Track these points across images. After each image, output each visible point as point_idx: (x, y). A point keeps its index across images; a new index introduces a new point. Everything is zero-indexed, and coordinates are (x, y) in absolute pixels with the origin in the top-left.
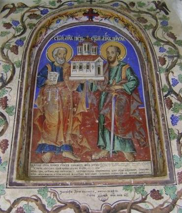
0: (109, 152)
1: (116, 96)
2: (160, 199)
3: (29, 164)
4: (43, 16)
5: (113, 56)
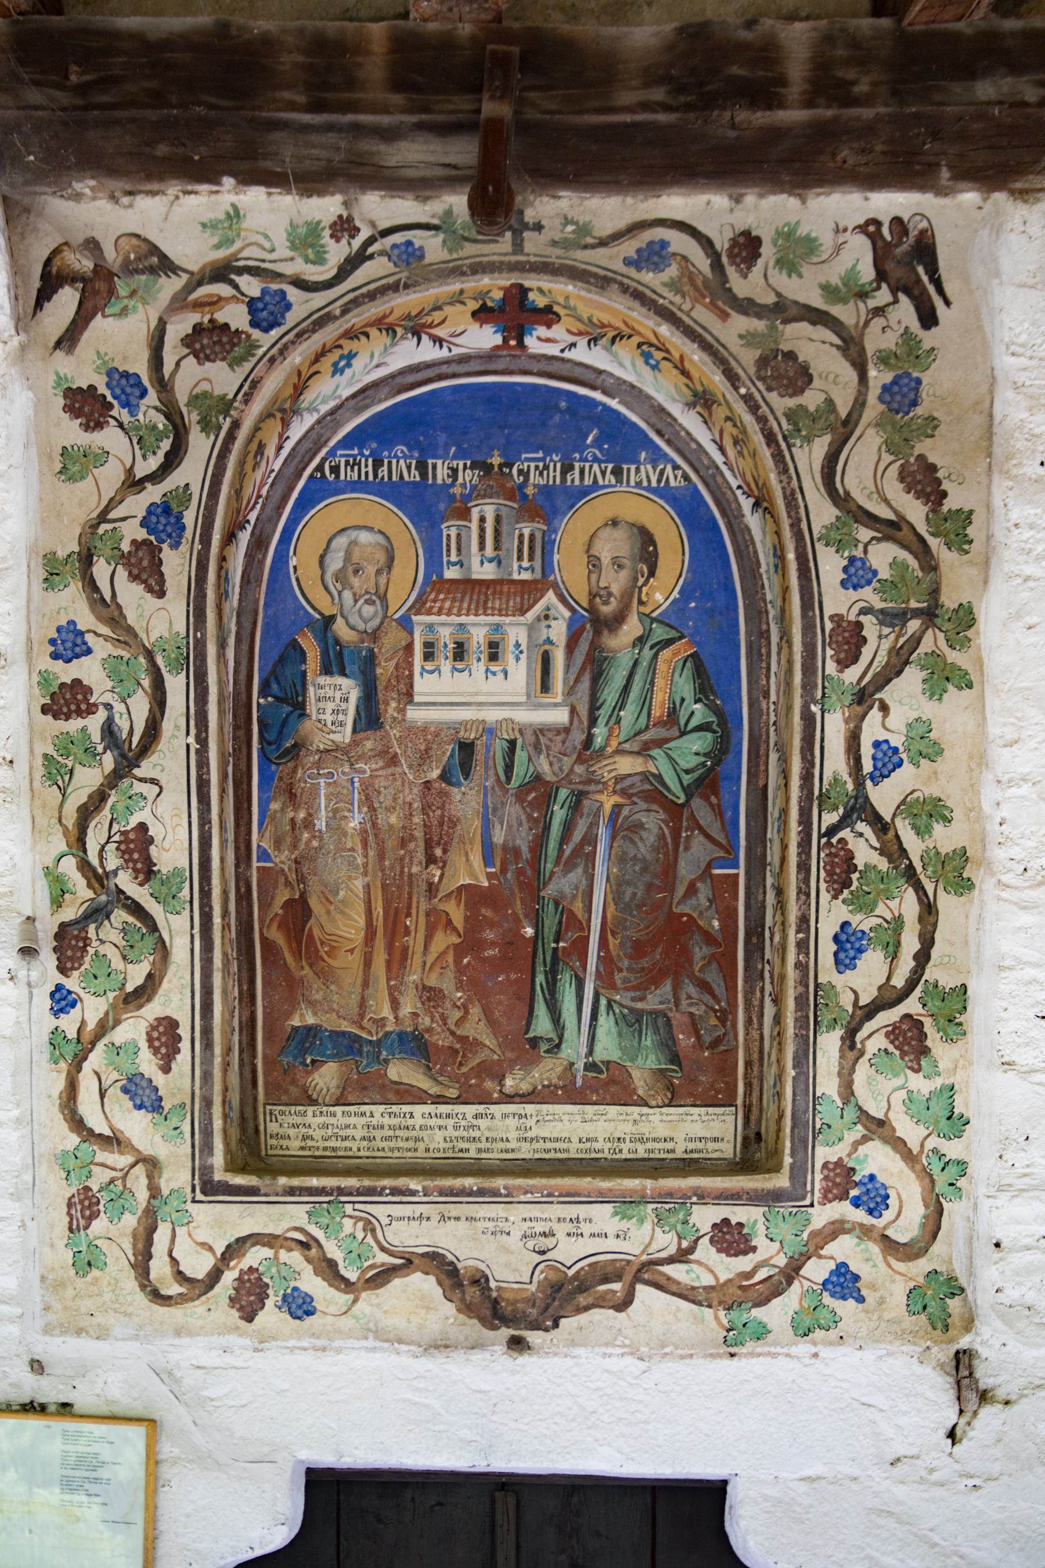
0: (572, 1064)
1: (617, 808)
2: (745, 1253)
3: (261, 1109)
4: (265, 340)
5: (616, 582)
